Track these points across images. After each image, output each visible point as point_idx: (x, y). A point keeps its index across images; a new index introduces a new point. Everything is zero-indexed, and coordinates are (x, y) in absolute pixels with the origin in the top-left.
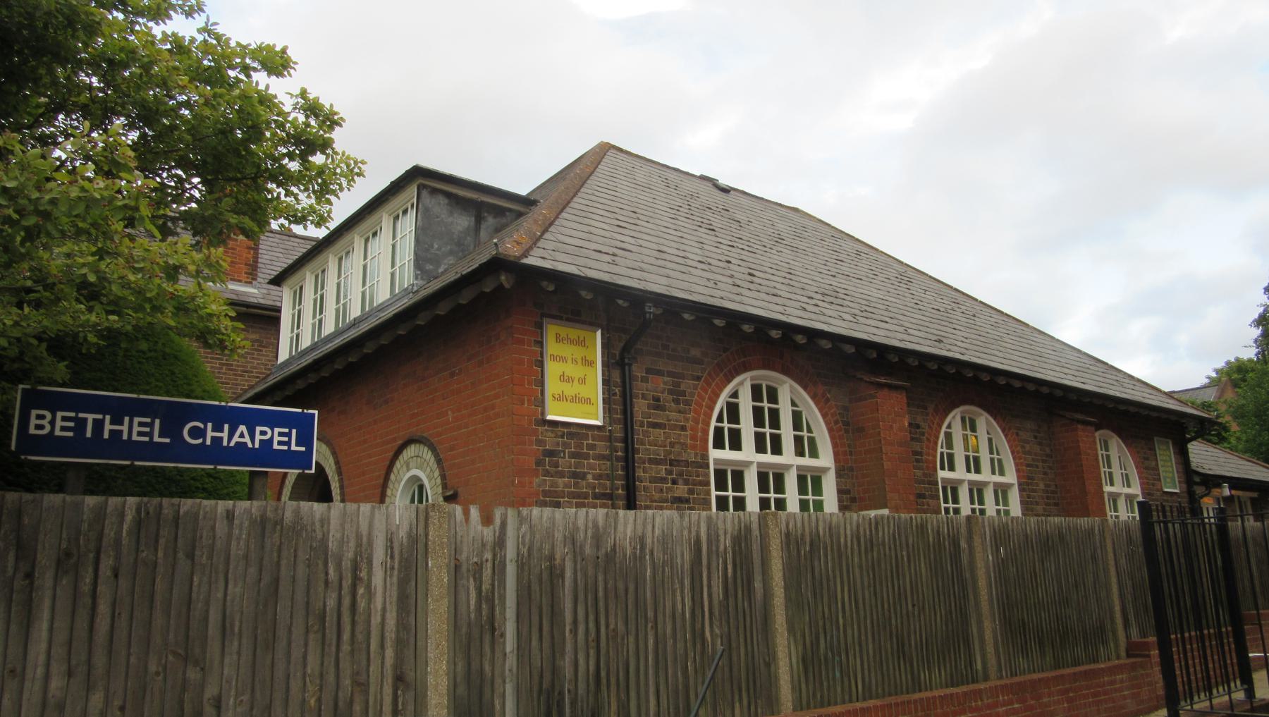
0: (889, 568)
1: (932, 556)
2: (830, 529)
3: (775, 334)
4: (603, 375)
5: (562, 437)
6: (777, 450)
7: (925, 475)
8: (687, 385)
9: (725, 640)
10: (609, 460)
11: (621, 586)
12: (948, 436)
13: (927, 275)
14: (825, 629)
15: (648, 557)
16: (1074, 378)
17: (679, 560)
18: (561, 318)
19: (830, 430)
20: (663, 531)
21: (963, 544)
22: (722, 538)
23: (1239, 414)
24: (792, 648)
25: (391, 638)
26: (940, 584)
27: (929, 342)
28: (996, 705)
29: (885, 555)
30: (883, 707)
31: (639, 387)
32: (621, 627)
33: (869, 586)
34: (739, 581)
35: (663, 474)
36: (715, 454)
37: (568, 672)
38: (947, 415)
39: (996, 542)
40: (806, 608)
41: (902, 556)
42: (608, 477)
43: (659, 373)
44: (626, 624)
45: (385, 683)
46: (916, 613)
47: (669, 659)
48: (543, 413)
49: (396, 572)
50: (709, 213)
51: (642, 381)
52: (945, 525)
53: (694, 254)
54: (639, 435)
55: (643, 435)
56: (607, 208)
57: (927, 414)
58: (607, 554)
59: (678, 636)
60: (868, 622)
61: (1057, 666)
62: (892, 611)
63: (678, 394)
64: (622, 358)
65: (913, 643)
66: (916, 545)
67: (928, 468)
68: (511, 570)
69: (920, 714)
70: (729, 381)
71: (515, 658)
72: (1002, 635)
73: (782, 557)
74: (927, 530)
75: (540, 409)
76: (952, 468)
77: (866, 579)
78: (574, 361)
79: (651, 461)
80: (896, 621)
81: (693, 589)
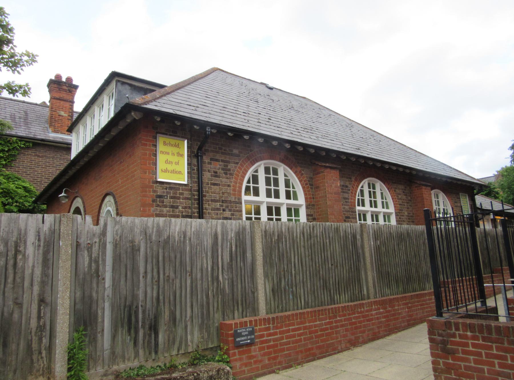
0: (319, 248)
1: (342, 242)
2: (288, 229)
3: (275, 143)
4: (188, 160)
5: (166, 189)
6: (277, 196)
7: (350, 208)
8: (231, 166)
9: (230, 281)
10: (190, 200)
11: (172, 255)
12: (362, 192)
13: (361, 125)
14: (285, 276)
15: (188, 242)
16: (423, 167)
17: (205, 243)
18: (167, 134)
19: (303, 188)
20: (197, 229)
21: (358, 237)
22: (230, 233)
23: (502, 187)
24: (267, 285)
25: (37, 281)
26: (346, 255)
27: (353, 149)
28: (371, 310)
29: (317, 241)
30: (311, 312)
31: (206, 167)
32: (172, 275)
33: (309, 256)
34: (238, 253)
35: (218, 206)
36: (358, 208)
37: (141, 296)
38: (361, 182)
39: (375, 237)
40: (275, 265)
41: (326, 242)
42: (190, 208)
43: (217, 160)
44: (175, 273)
45: (33, 303)
46: (333, 268)
47: (199, 290)
48: (156, 178)
49: (42, 248)
50: (259, 96)
51: (208, 164)
52: (349, 228)
53: (242, 109)
54: (206, 188)
55: (208, 189)
56: (204, 90)
57: (352, 181)
58: (165, 240)
59: (204, 280)
60: (308, 272)
61: (405, 292)
62: (321, 267)
63: (226, 171)
64: (198, 153)
65: (331, 282)
66: (334, 237)
67: (351, 205)
68: (109, 248)
69: (331, 315)
70: (253, 165)
71: (111, 290)
72: (377, 278)
73: (262, 242)
74: (340, 230)
75: (155, 176)
76: (363, 205)
77: (307, 253)
78: (173, 154)
79: (212, 201)
80: (323, 272)
81: (213, 257)
